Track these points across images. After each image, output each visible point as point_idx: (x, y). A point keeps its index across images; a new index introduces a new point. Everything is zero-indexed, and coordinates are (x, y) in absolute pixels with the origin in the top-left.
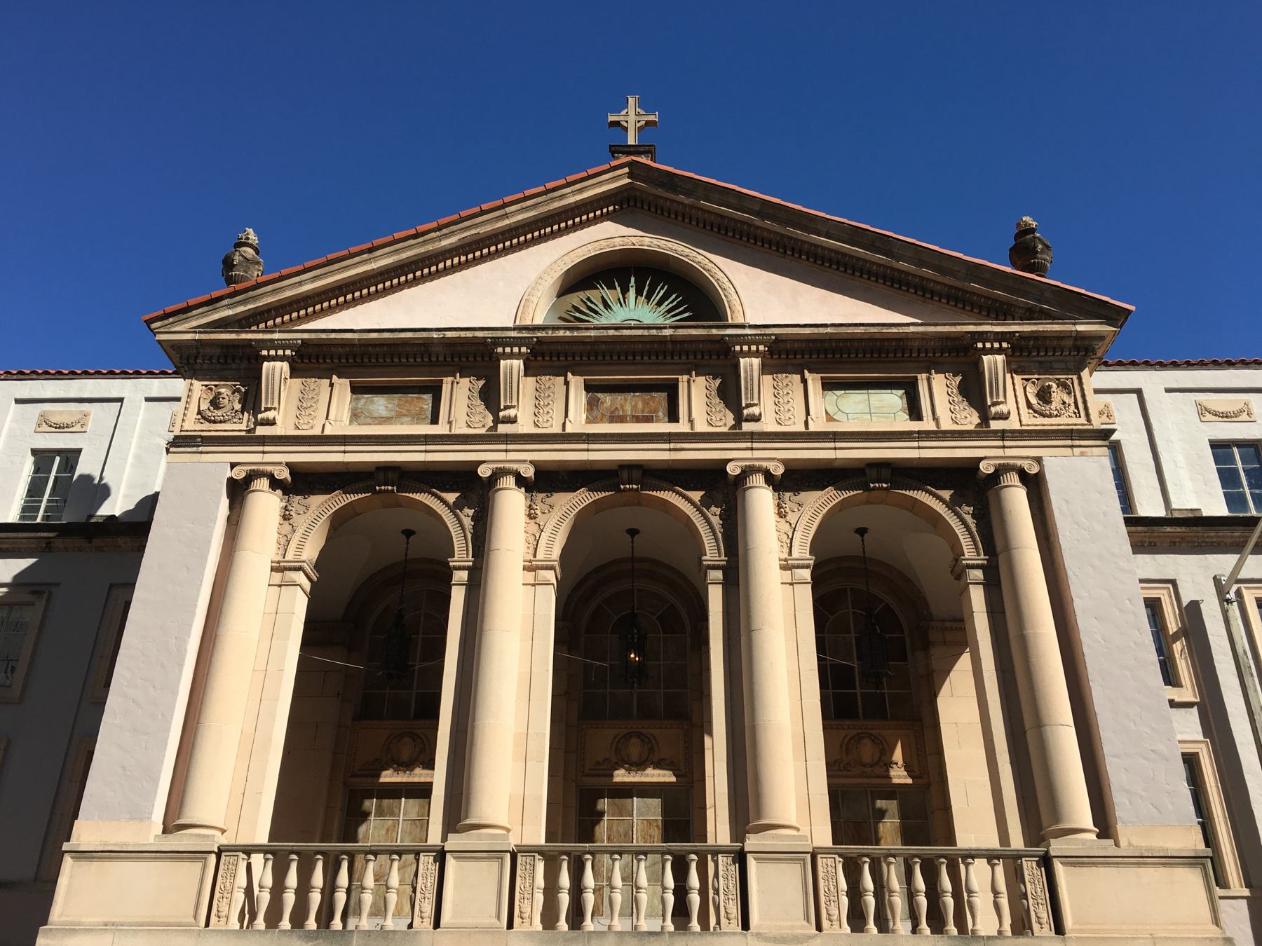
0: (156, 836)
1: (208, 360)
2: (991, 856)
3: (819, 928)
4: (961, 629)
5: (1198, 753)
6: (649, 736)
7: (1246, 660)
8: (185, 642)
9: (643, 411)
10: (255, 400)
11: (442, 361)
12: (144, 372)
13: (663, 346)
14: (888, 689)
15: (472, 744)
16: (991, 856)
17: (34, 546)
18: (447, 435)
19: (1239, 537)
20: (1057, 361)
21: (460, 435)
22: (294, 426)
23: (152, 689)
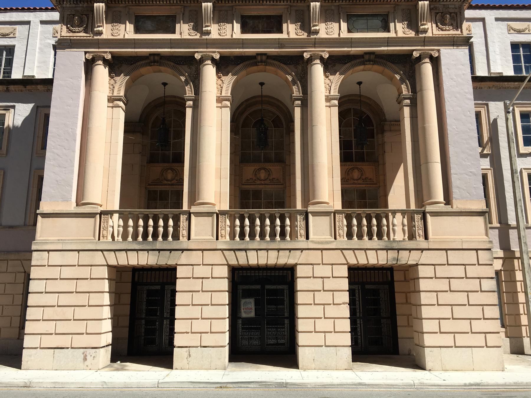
0: (74, 207)
2: (403, 212)
3: (335, 238)
5: (487, 173)
7: (512, 136)
8: (76, 130)
10: (92, 22)
11: (175, 3)
12: (38, 8)
14: (366, 150)
15: (199, 172)
16: (403, 212)
17: (1, 89)
18: (180, 39)
19: (517, 85)
20: (451, 5)
21: (186, 39)
22: (111, 35)
23: (64, 150)
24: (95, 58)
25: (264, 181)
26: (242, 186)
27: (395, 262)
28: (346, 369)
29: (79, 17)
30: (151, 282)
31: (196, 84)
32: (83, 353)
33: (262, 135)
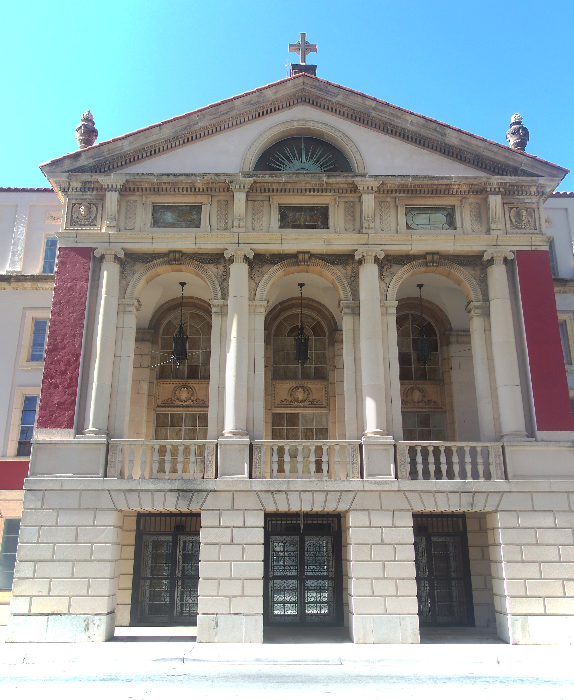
1: (75, 189)
4: (468, 335)
6: (308, 388)
9: (310, 222)
13: (321, 185)
20: (527, 198)
24: (105, 256)
25: (302, 402)
26: (275, 409)
27: (469, 508)
28: (412, 643)
29: (86, 206)
30: (165, 531)
31: (225, 287)
32: (85, 621)
33: (302, 346)
